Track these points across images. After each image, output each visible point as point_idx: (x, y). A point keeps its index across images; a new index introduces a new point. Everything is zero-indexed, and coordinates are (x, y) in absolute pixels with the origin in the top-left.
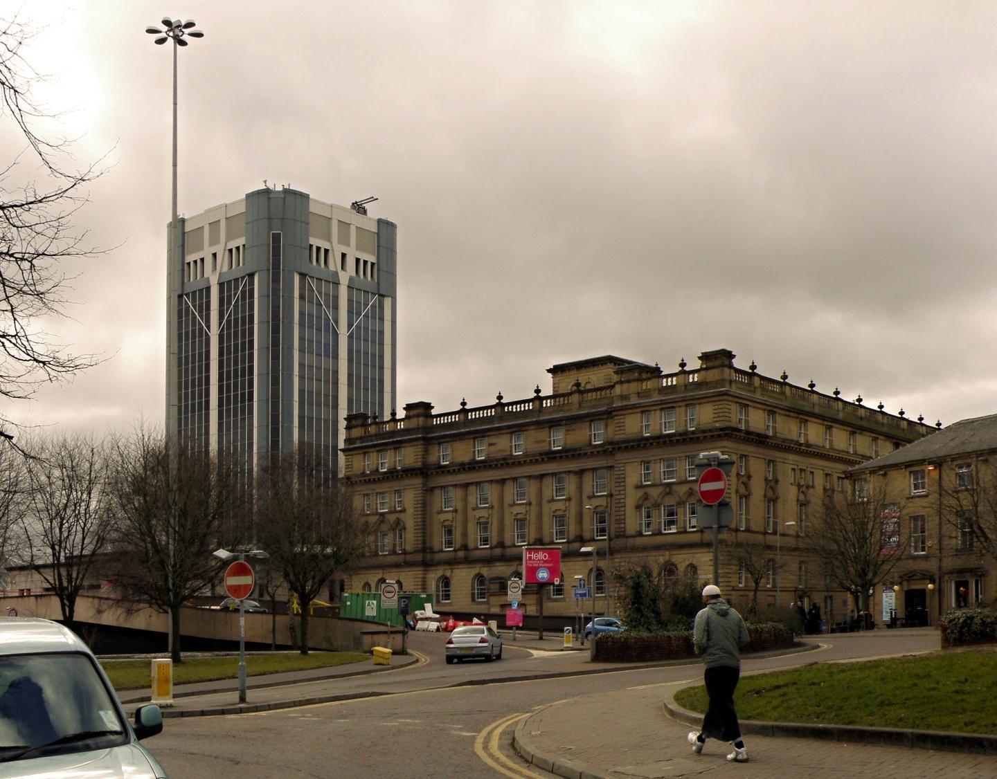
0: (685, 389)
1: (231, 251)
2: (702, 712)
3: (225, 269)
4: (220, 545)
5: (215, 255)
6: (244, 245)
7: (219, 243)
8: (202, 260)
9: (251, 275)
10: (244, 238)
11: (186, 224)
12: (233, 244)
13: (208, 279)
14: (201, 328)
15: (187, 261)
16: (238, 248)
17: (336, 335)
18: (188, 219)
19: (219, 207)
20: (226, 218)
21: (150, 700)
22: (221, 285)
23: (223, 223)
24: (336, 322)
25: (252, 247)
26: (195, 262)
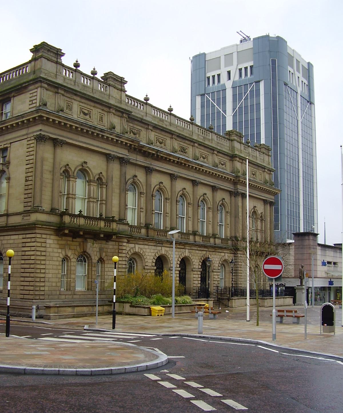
0: (179, 158)
1: (240, 70)
2: (271, 338)
3: (237, 78)
4: (11, 248)
5: (229, 73)
6: (251, 67)
7: (232, 65)
8: (219, 75)
9: (258, 82)
10: (253, 62)
11: (207, 56)
12: (242, 66)
13: (224, 85)
14: (219, 112)
15: (208, 75)
16: (246, 68)
17: (224, 118)
18: (207, 54)
19: (233, 46)
20: (237, 52)
21: (322, 325)
22: (234, 88)
23: (235, 56)
24: (225, 111)
25: (196, 70)
26: (214, 77)
